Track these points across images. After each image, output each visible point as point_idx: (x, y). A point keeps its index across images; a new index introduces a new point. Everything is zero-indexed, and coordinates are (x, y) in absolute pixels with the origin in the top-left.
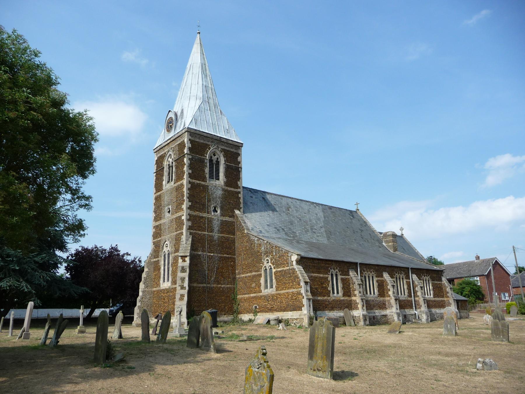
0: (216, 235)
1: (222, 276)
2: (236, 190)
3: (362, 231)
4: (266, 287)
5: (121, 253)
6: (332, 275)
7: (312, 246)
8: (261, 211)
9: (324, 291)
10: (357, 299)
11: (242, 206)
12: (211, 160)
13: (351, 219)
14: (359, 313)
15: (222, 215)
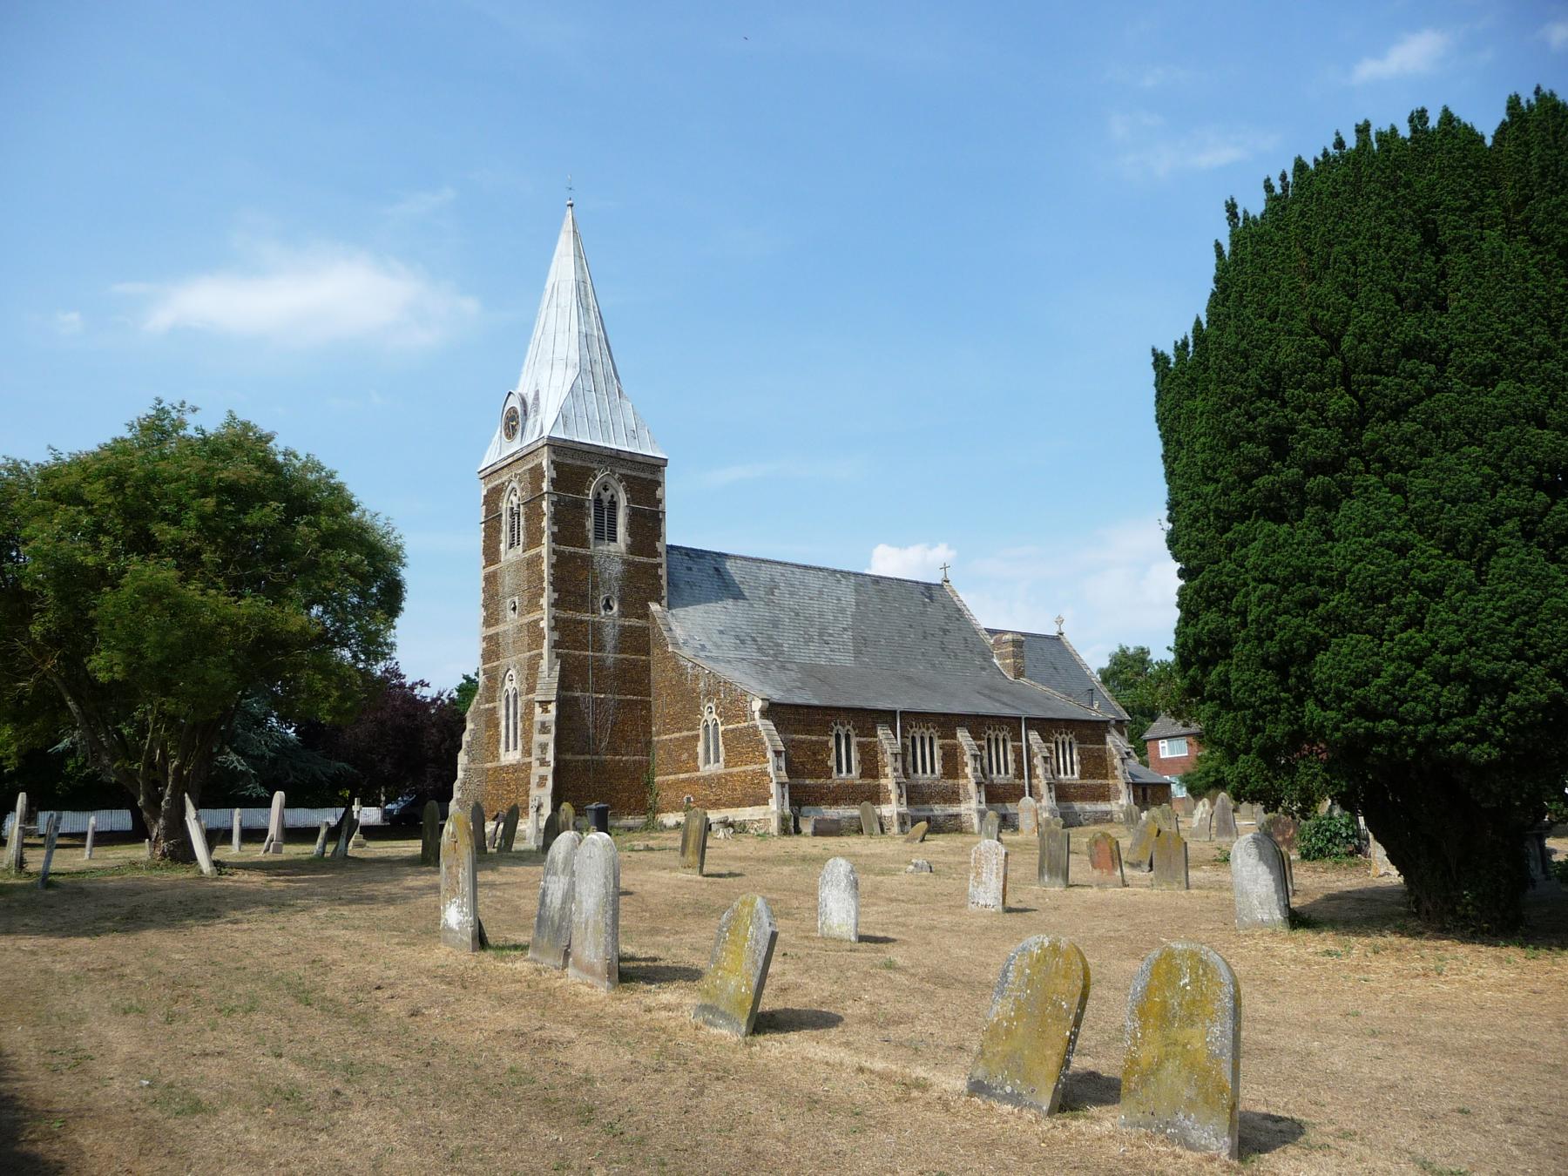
0: (610, 657)
1: (623, 738)
2: (652, 560)
3: (945, 631)
4: (707, 761)
5: (408, 681)
6: (838, 737)
7: (810, 672)
8: (708, 600)
9: (819, 769)
10: (889, 782)
11: (664, 593)
12: (598, 501)
13: (924, 604)
14: (891, 809)
15: (623, 615)
